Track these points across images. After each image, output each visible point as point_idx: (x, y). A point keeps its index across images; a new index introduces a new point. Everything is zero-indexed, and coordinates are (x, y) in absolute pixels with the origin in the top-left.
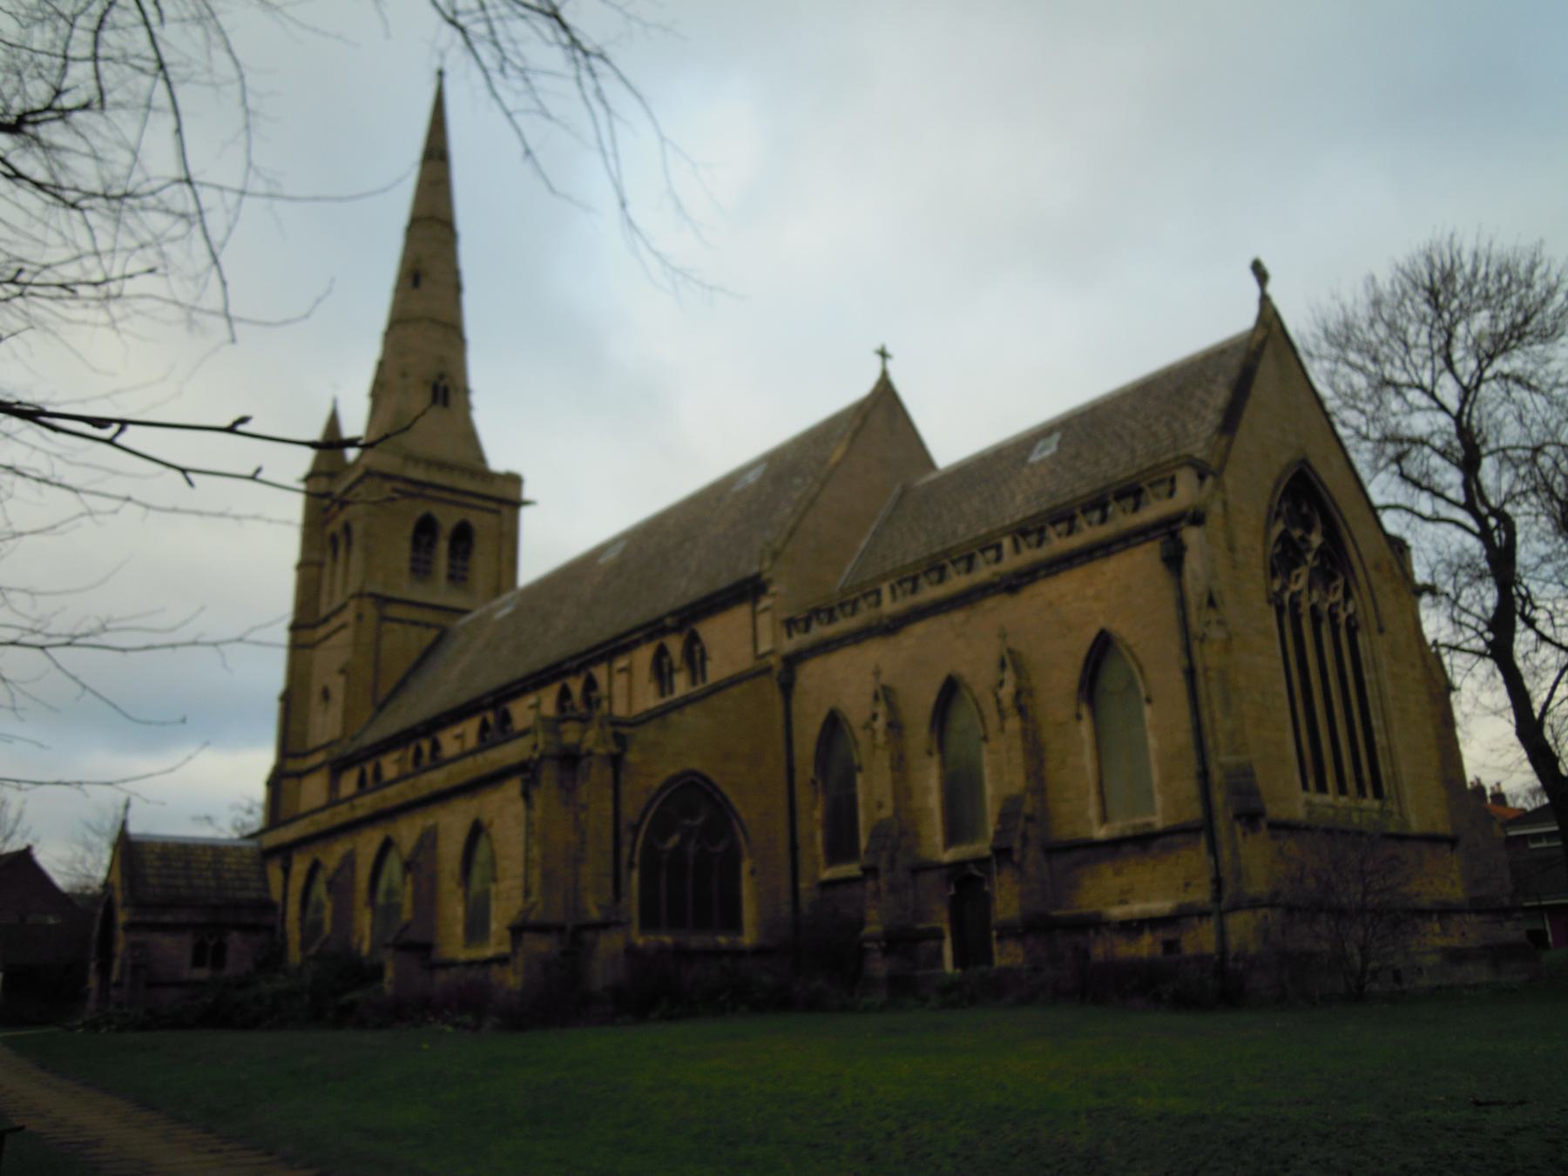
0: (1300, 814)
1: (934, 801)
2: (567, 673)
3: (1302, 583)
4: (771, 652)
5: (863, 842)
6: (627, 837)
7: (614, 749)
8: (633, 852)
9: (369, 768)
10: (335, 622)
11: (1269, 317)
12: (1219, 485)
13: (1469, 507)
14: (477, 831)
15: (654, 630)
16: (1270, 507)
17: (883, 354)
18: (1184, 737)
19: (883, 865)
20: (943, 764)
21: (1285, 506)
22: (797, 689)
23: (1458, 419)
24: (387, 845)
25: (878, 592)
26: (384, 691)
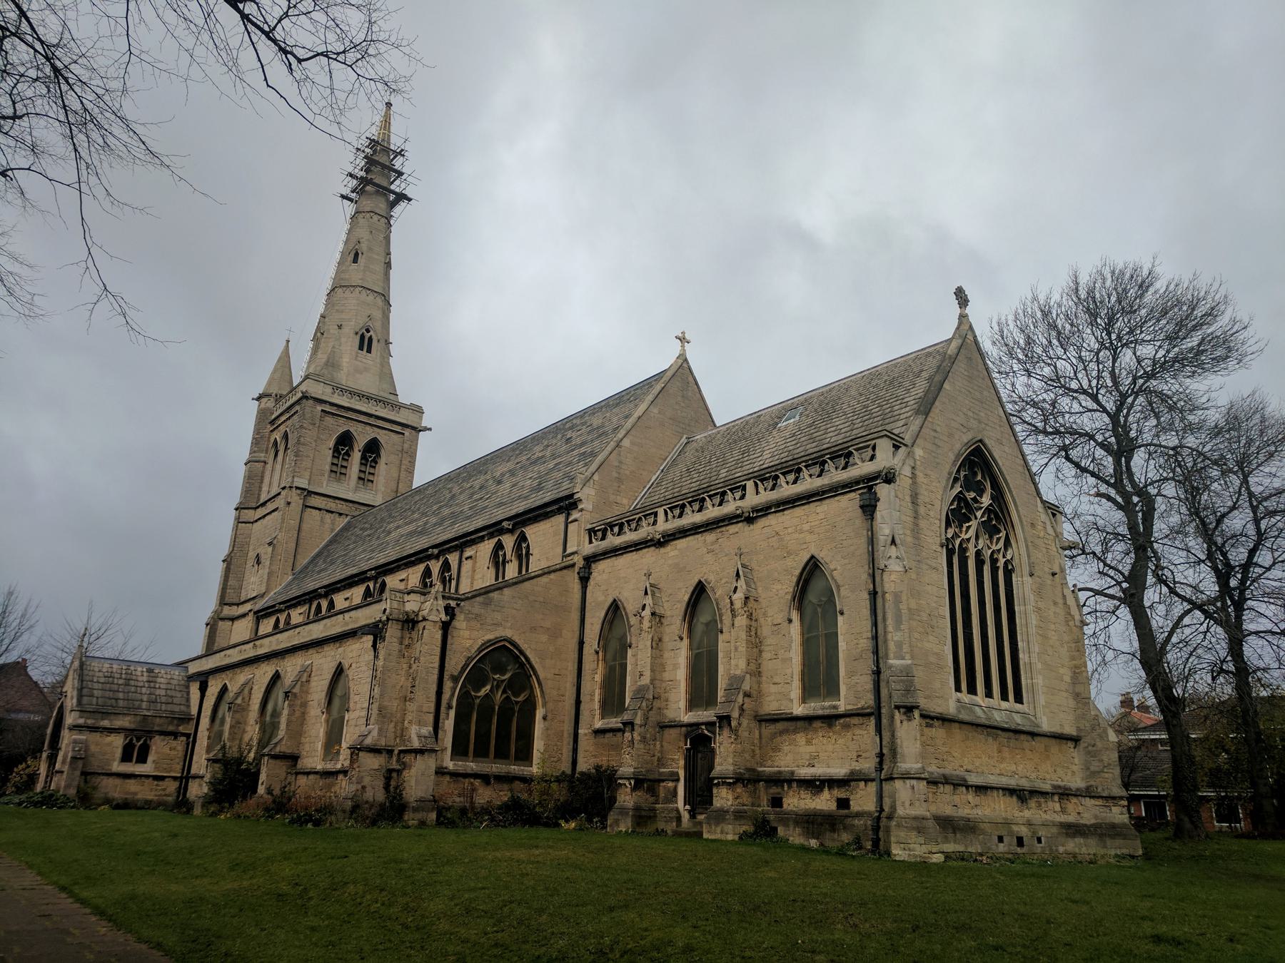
1: (681, 675)
2: (430, 557)
3: (972, 533)
5: (720, 693)
6: (448, 684)
7: (444, 618)
8: (453, 695)
9: (282, 617)
10: (270, 506)
11: (965, 329)
13: (1118, 486)
14: (339, 671)
15: (495, 529)
16: (950, 474)
17: (683, 339)
18: (865, 643)
19: (638, 721)
20: (691, 648)
21: (962, 474)
22: (591, 583)
23: (1114, 417)
24: (276, 677)
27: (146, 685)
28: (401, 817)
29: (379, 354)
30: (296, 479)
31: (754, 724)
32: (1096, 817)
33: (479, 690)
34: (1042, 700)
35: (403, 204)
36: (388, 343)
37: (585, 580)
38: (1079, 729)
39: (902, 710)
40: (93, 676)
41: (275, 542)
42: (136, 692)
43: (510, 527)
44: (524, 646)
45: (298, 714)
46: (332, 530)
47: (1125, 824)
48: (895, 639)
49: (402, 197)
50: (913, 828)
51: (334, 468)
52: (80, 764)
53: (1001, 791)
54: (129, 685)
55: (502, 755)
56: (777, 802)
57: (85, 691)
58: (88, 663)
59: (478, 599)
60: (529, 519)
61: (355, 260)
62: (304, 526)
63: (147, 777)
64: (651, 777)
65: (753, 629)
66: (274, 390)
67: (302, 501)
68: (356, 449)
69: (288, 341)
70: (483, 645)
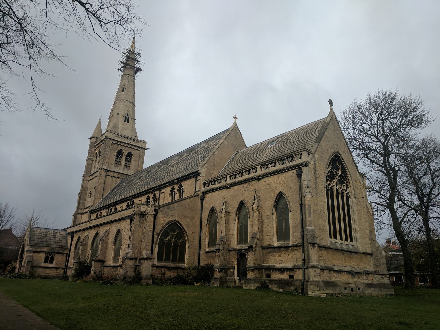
0: (328, 244)
2: (149, 193)
3: (335, 183)
4: (199, 191)
6: (156, 236)
8: (157, 240)
9: (99, 213)
10: (95, 175)
12: (313, 157)
13: (385, 167)
14: (119, 232)
15: (171, 183)
16: (327, 163)
17: (235, 118)
18: (299, 222)
19: (221, 248)
20: (239, 223)
22: (205, 201)
23: (383, 144)
24: (97, 234)
25: (226, 178)
26: (106, 194)
27: (53, 236)
28: (140, 282)
29: (131, 123)
30: (103, 166)
31: (261, 250)
32: (378, 281)
33: (166, 238)
34: (359, 241)
35: (139, 72)
36: (134, 119)
37: (202, 200)
38: (372, 251)
39: (311, 245)
40: (35, 234)
41: (96, 188)
42: (49, 239)
43: (177, 182)
44: (182, 223)
45: (104, 246)
46: (116, 183)
47: (388, 284)
48: (309, 220)
49: (139, 69)
50: (315, 285)
51: (116, 162)
52: (30, 264)
53: (345, 272)
54: (47, 237)
55: (174, 260)
56: (269, 276)
57: (32, 239)
58: (33, 229)
59: (166, 207)
60: (183, 179)
61: (123, 91)
62: (107, 182)
63: (53, 268)
64: (225, 268)
65: (260, 217)
66: (96, 136)
67: (105, 174)
68: (124, 156)
69: (100, 119)
70: (168, 222)
